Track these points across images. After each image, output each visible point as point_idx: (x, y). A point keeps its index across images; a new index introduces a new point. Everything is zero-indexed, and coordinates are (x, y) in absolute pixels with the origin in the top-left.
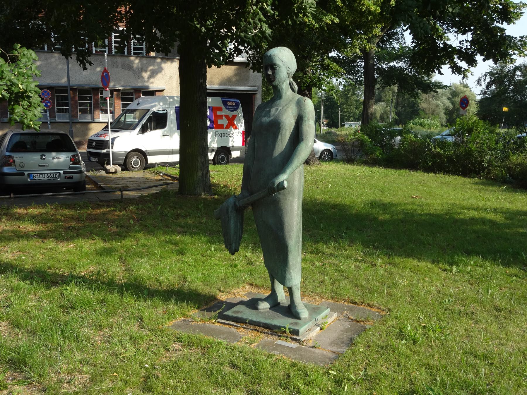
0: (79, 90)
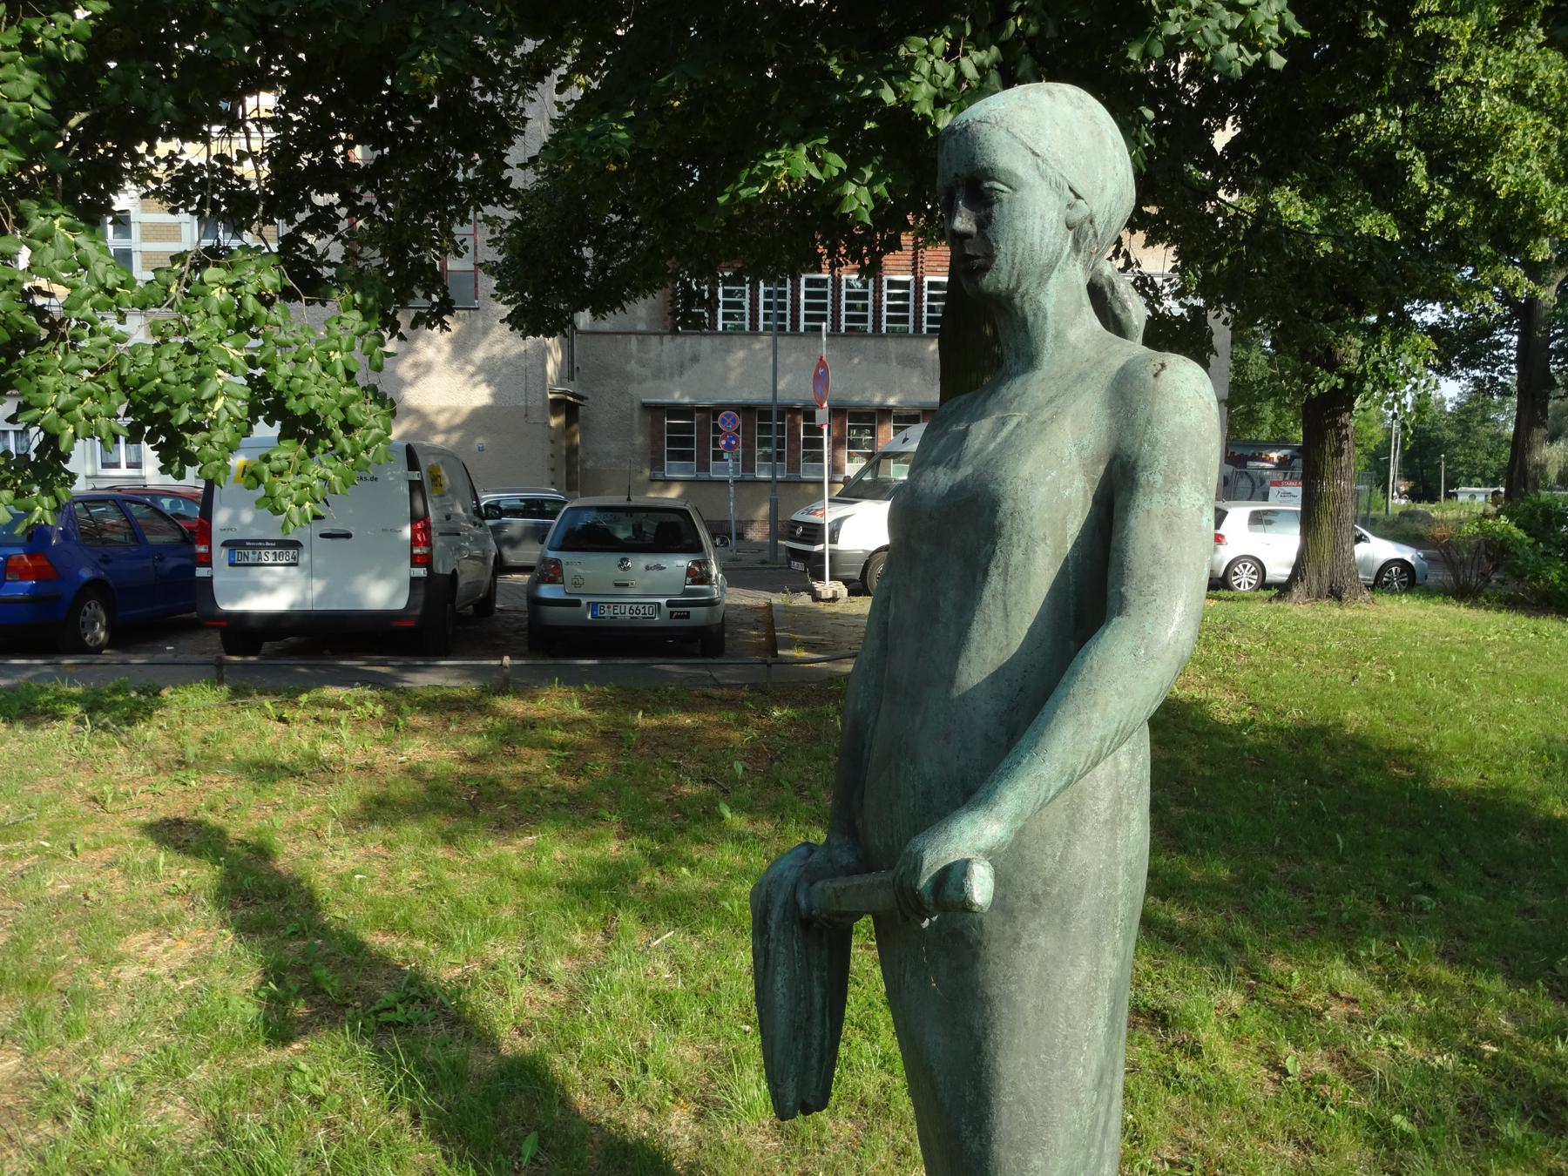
0: (851, 413)
